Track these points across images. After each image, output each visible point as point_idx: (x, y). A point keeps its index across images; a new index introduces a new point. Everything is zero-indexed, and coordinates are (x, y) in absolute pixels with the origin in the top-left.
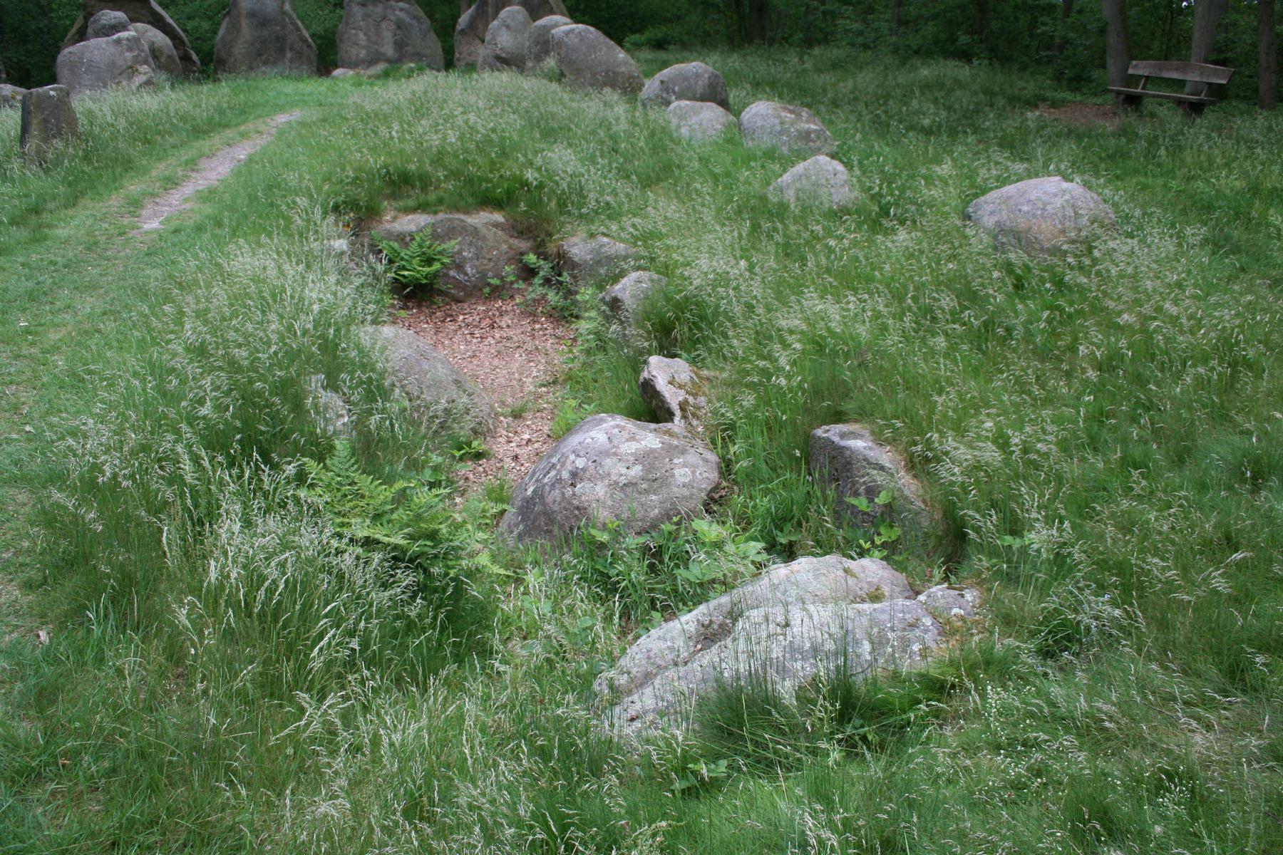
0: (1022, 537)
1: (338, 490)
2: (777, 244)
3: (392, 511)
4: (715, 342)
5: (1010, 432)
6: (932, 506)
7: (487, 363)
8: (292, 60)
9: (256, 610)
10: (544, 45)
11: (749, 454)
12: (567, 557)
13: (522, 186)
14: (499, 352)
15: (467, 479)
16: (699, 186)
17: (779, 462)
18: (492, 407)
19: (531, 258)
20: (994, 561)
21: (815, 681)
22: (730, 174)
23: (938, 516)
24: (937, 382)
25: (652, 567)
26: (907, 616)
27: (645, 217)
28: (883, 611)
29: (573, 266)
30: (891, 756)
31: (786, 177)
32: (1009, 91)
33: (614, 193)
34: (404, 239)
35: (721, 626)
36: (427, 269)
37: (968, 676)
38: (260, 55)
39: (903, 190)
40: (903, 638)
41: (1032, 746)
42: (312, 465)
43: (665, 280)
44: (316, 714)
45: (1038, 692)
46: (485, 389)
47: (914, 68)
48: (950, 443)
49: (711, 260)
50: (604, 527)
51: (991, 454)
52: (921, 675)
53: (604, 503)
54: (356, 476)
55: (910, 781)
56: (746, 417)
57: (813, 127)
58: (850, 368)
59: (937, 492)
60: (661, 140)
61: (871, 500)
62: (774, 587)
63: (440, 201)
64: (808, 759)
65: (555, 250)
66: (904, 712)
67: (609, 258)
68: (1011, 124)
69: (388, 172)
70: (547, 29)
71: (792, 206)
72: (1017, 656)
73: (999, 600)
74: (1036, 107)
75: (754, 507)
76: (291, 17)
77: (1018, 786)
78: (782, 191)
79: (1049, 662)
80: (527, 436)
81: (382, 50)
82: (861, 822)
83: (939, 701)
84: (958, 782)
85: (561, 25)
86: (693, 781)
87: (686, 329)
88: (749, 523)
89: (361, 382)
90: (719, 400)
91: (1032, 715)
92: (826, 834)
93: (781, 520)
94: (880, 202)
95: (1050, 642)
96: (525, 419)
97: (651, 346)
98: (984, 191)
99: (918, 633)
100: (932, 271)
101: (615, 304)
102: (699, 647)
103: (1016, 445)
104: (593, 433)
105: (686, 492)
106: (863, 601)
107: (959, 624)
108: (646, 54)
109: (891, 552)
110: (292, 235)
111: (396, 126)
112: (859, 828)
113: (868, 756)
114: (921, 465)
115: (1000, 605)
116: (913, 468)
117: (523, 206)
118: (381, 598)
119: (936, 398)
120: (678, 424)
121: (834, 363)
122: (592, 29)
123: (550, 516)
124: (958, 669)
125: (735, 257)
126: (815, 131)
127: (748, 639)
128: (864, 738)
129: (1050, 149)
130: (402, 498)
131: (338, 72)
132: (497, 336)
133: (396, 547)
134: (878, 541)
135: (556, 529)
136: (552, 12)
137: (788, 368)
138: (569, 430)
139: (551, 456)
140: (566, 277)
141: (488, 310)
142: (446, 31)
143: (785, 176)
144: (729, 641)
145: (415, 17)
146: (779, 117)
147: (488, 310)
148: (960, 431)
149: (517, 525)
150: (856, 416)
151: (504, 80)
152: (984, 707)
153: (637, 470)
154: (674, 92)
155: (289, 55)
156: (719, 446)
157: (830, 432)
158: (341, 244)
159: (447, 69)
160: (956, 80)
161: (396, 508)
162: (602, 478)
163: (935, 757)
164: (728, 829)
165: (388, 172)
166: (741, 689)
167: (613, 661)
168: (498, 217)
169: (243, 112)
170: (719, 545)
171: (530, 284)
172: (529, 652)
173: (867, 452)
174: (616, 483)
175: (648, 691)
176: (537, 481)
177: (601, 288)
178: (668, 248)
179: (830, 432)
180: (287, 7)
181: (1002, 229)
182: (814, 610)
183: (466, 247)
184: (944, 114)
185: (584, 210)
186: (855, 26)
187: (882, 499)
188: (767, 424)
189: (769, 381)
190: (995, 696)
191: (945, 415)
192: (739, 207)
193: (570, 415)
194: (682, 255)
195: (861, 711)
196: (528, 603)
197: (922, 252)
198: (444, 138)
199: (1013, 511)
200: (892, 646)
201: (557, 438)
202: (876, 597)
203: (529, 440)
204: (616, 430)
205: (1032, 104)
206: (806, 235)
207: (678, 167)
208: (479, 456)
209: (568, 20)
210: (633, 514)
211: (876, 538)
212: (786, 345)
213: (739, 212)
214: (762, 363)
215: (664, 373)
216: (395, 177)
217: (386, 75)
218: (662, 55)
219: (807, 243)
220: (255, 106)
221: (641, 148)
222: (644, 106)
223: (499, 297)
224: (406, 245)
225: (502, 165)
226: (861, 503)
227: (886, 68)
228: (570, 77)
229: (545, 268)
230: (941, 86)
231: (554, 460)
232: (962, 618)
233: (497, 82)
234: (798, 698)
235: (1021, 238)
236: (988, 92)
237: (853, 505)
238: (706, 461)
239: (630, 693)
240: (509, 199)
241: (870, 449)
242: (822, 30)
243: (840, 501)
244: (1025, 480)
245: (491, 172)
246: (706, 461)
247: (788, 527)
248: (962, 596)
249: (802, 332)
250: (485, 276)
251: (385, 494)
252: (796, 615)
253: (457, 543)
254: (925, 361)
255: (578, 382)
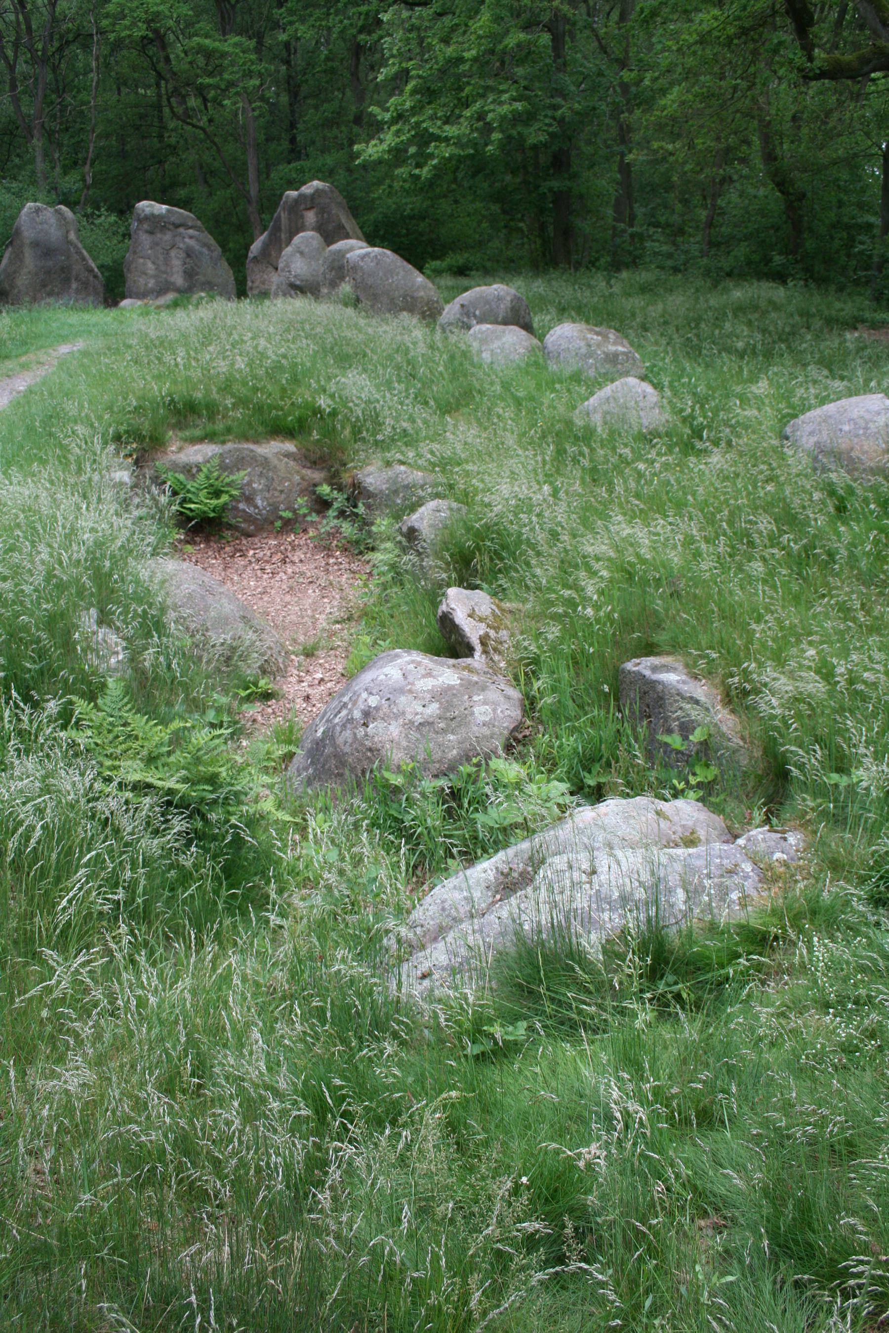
0: (849, 774)
1: (109, 731)
2: (583, 469)
3: (169, 753)
4: (517, 571)
5: (835, 661)
6: (752, 743)
7: (277, 599)
8: (78, 291)
9: (8, 860)
10: (339, 270)
11: (554, 690)
12: (356, 801)
13: (315, 413)
14: (291, 588)
15: (254, 721)
16: (501, 411)
17: (586, 698)
18: (283, 646)
19: (325, 489)
20: (819, 801)
21: (624, 932)
22: (539, 404)
23: (758, 753)
24: (754, 610)
25: (449, 811)
26: (725, 862)
27: (444, 442)
28: (698, 857)
29: (370, 495)
30: (708, 1015)
31: (593, 401)
32: (826, 313)
33: (412, 420)
34: (189, 470)
35: (521, 874)
36: (214, 502)
37: (792, 926)
38: (44, 286)
39: (716, 411)
40: (720, 885)
41: (865, 1004)
42: (81, 706)
43: (464, 509)
44: (64, 971)
45: (870, 944)
46: (276, 626)
47: (726, 290)
48: (769, 673)
49: (512, 486)
50: (399, 770)
51: (815, 687)
52: (741, 927)
53: (398, 744)
54: (129, 717)
55: (728, 1044)
56: (550, 650)
57: (621, 349)
58: (661, 597)
59: (757, 728)
60: (460, 364)
61: (685, 738)
62: (581, 832)
63: (229, 430)
64: (614, 1021)
65: (350, 480)
66: (722, 966)
67: (407, 487)
68: (831, 343)
69: (172, 400)
70: (341, 254)
71: (599, 429)
72: (847, 903)
73: (824, 843)
74: (856, 329)
75: (560, 747)
76: (76, 247)
77: (848, 1049)
78: (588, 414)
79: (881, 911)
80: (319, 676)
81: (172, 279)
82: (675, 1090)
83: (760, 954)
84: (782, 1044)
85: (356, 249)
86: (488, 1046)
87: (487, 560)
88: (555, 765)
89: (136, 615)
90: (522, 633)
91: (863, 969)
92: (633, 1106)
93: (589, 760)
94: (691, 425)
95: (882, 888)
96: (318, 657)
97: (450, 577)
98: (805, 408)
99: (736, 879)
100: (749, 494)
101: (412, 534)
102: (498, 897)
103: (842, 675)
104: (387, 670)
105: (486, 731)
106: (677, 845)
107: (782, 869)
108: (448, 281)
109: (707, 793)
110: (67, 464)
111: (181, 352)
112: (673, 1097)
113: (682, 1016)
114: (738, 698)
115: (827, 849)
116: (730, 702)
117: (315, 435)
118: (152, 845)
119: (754, 626)
120: (478, 659)
121: (644, 592)
122: (388, 252)
123: (340, 759)
124: (781, 918)
125: (538, 483)
126: (624, 353)
127: (550, 889)
128: (678, 997)
129: (871, 370)
130: (178, 740)
131: (125, 303)
132: (290, 571)
133: (171, 792)
134: (693, 781)
135: (347, 772)
136: (347, 237)
137: (595, 597)
138: (363, 667)
139: (343, 695)
140: (361, 509)
141: (280, 545)
142: (238, 261)
143: (591, 400)
144: (529, 889)
145: (205, 245)
146: (585, 339)
147: (280, 545)
148: (780, 661)
149: (306, 769)
150: (667, 648)
151: (300, 304)
152: (811, 960)
153: (434, 709)
154: (475, 316)
155: (74, 286)
156: (522, 682)
157: (642, 666)
158: (124, 476)
159: (239, 297)
160: (770, 302)
161: (173, 751)
162: (396, 717)
163: (757, 1017)
164: (525, 1101)
165: (172, 400)
166: (542, 943)
167: (401, 912)
168: (290, 446)
169: (24, 343)
170: (518, 786)
171: (324, 517)
172: (308, 904)
173: (680, 686)
174: (411, 722)
175: (441, 945)
176: (328, 721)
177: (397, 517)
178: (467, 474)
179: (642, 666)
180: (72, 236)
181: (820, 448)
182: (624, 856)
183: (256, 479)
184: (759, 337)
185: (379, 437)
186: (665, 248)
187: (697, 736)
188: (573, 658)
189: (575, 611)
190: (822, 949)
191: (764, 645)
192: (543, 432)
193: (365, 652)
194: (482, 481)
195: (676, 967)
196: (309, 849)
197: (737, 475)
198: (233, 365)
199: (839, 747)
200: (709, 895)
201: (349, 676)
202: (690, 841)
203: (322, 680)
204: (412, 666)
205: (853, 324)
206: (614, 460)
207: (479, 392)
208: (267, 696)
209: (364, 244)
210: (430, 756)
211: (691, 778)
212: (593, 573)
213: (543, 437)
214: (567, 593)
215: (464, 605)
216: (180, 406)
217: (175, 305)
218: (464, 281)
219: (616, 467)
220: (37, 337)
221: (441, 374)
222: (444, 331)
223: (292, 531)
224: (193, 477)
225: (294, 392)
226: (675, 741)
227: (697, 290)
228: (366, 303)
229: (339, 500)
230: (756, 308)
231: (346, 699)
232: (785, 864)
233: (289, 308)
234: (605, 952)
235: (844, 458)
236: (804, 314)
237: (666, 744)
238: (508, 698)
239: (423, 947)
240: (301, 427)
241: (684, 682)
242: (630, 253)
243: (652, 740)
244: (851, 712)
245: (282, 399)
246: (508, 698)
247: (596, 768)
248: (785, 839)
249: (610, 559)
250: (277, 509)
251: (160, 735)
252: (603, 861)
253: (238, 788)
254: (742, 588)
255: (373, 618)
